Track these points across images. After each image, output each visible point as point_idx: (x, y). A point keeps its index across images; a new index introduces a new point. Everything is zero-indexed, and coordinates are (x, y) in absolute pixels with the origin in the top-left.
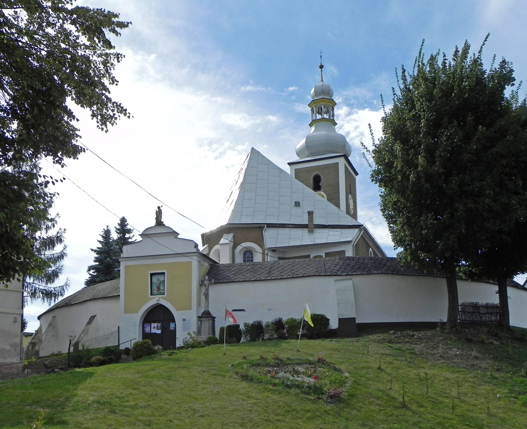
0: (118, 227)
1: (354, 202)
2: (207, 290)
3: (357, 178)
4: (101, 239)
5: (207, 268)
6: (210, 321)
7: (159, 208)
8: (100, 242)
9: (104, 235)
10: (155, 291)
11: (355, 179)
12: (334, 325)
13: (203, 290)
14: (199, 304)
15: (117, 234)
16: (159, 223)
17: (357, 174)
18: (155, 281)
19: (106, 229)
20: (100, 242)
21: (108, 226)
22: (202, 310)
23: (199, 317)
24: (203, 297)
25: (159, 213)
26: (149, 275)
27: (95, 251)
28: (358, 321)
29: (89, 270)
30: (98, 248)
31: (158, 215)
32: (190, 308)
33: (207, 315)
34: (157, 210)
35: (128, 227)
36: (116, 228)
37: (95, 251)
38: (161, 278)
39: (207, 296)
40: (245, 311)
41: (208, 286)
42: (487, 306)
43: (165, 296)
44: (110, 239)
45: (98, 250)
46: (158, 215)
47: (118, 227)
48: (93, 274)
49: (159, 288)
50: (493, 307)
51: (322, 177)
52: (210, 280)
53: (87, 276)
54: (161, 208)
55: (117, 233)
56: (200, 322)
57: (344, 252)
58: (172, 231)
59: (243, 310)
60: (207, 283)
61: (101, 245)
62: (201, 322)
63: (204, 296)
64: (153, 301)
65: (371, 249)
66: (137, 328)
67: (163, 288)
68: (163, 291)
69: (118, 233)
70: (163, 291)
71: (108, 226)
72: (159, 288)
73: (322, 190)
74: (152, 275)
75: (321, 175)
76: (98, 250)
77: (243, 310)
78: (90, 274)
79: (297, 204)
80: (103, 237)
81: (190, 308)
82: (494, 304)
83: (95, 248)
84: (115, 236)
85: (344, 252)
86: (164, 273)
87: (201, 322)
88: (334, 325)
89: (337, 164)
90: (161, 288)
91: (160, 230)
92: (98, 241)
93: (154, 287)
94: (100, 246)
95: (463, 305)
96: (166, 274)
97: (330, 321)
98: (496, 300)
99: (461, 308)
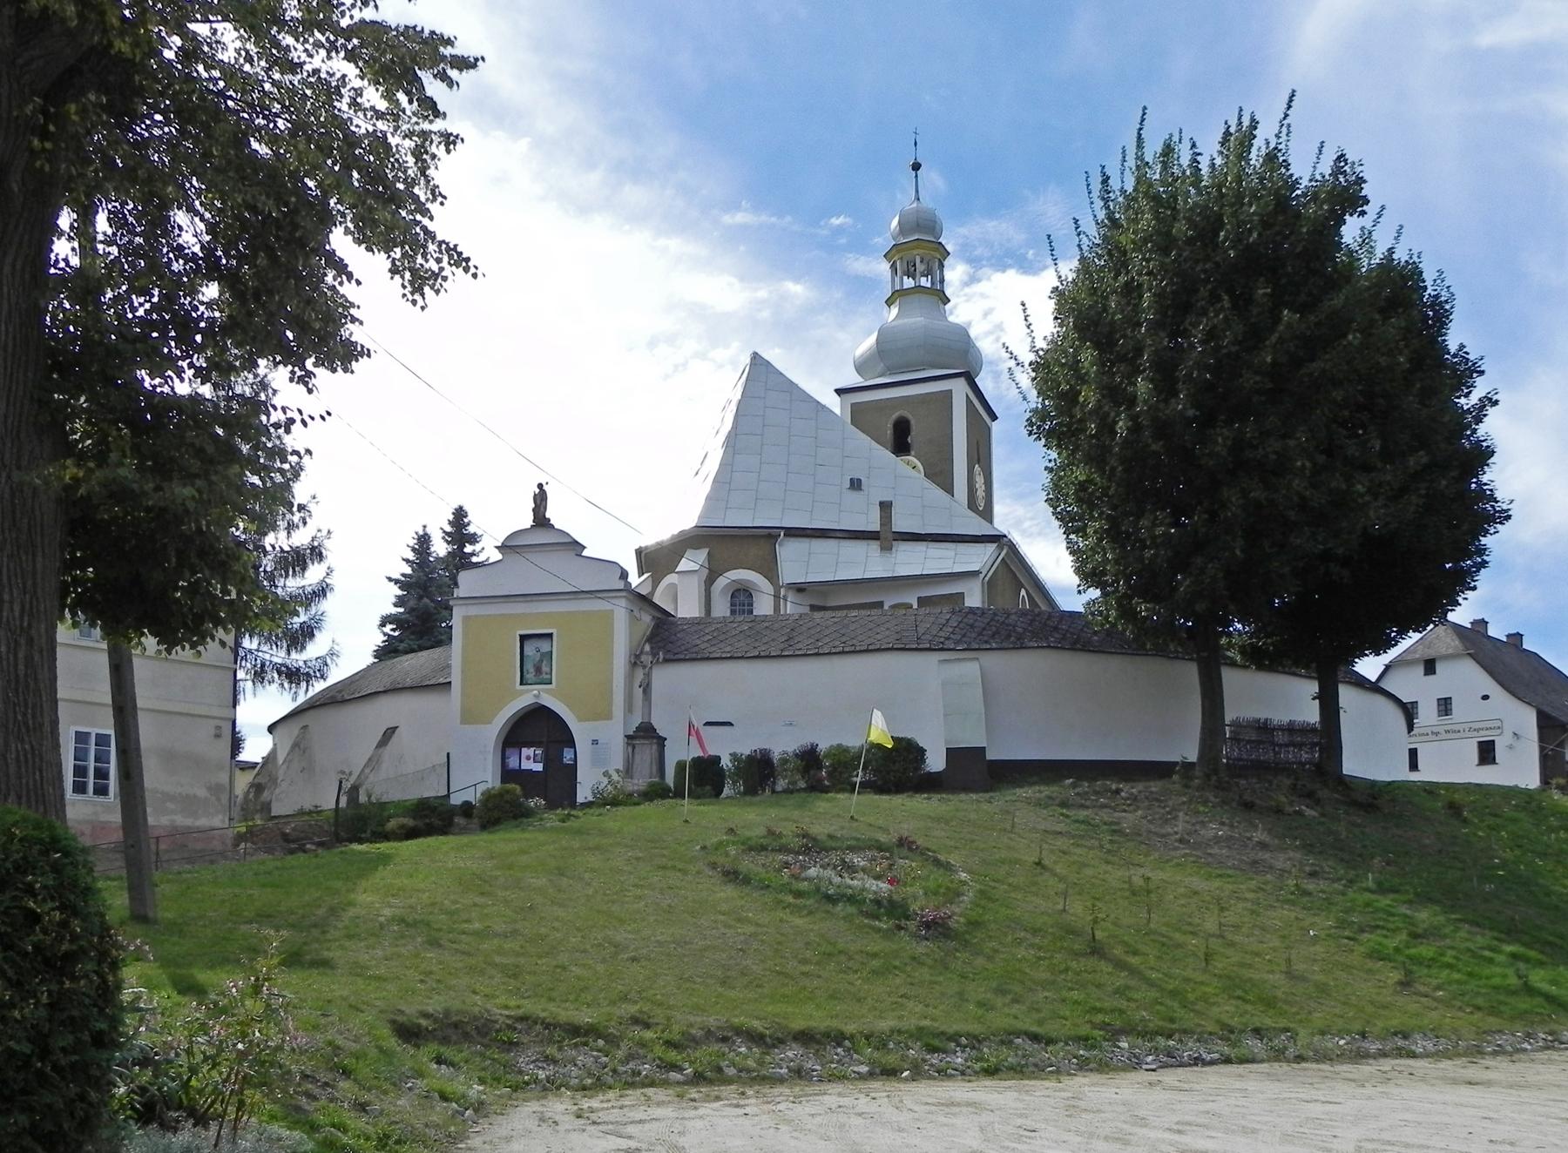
0: (449, 529)
1: (985, 483)
2: (648, 675)
3: (996, 427)
4: (411, 556)
5: (648, 627)
6: (655, 747)
7: (540, 486)
8: (407, 561)
9: (417, 547)
10: (530, 676)
11: (989, 429)
12: (936, 762)
13: (639, 675)
14: (629, 708)
15: (445, 545)
16: (541, 521)
17: (994, 417)
18: (530, 654)
19: (421, 533)
20: (407, 561)
21: (425, 527)
22: (637, 721)
23: (628, 737)
24: (639, 692)
25: (541, 499)
26: (518, 639)
27: (397, 582)
28: (990, 756)
29: (383, 625)
30: (403, 575)
31: (538, 502)
32: (608, 716)
33: (646, 734)
34: (537, 491)
35: (471, 529)
36: (444, 532)
37: (397, 582)
38: (544, 646)
39: (647, 689)
40: (393, 729)
41: (651, 668)
42: (1291, 729)
43: (553, 686)
44: (429, 554)
45: (403, 579)
46: (538, 502)
47: (449, 529)
48: (392, 633)
49: (538, 670)
50: (1306, 730)
51: (913, 422)
52: (654, 654)
53: (378, 639)
54: (545, 487)
55: (447, 541)
56: (630, 749)
57: (961, 596)
58: (570, 540)
59: (730, 724)
60: (646, 659)
61: (410, 569)
62: (634, 748)
63: (641, 689)
64: (526, 698)
65: (1023, 592)
66: (490, 757)
67: (548, 670)
68: (548, 676)
69: (448, 543)
70: (548, 676)
71: (425, 527)
72: (538, 670)
73: (913, 453)
74: (523, 638)
75: (910, 417)
76: (403, 579)
77: (730, 724)
78: (385, 634)
79: (856, 485)
80: (414, 550)
81: (608, 716)
82: (1308, 724)
83: (397, 576)
84: (440, 548)
85: (961, 596)
86: (550, 636)
87: (634, 748)
88: (936, 762)
89: (948, 394)
90: (545, 668)
91: (542, 537)
92: (404, 560)
93: (529, 667)
94: (408, 571)
95: (1236, 724)
96: (555, 638)
97: (927, 754)
98: (1311, 714)
99: (1231, 732)
